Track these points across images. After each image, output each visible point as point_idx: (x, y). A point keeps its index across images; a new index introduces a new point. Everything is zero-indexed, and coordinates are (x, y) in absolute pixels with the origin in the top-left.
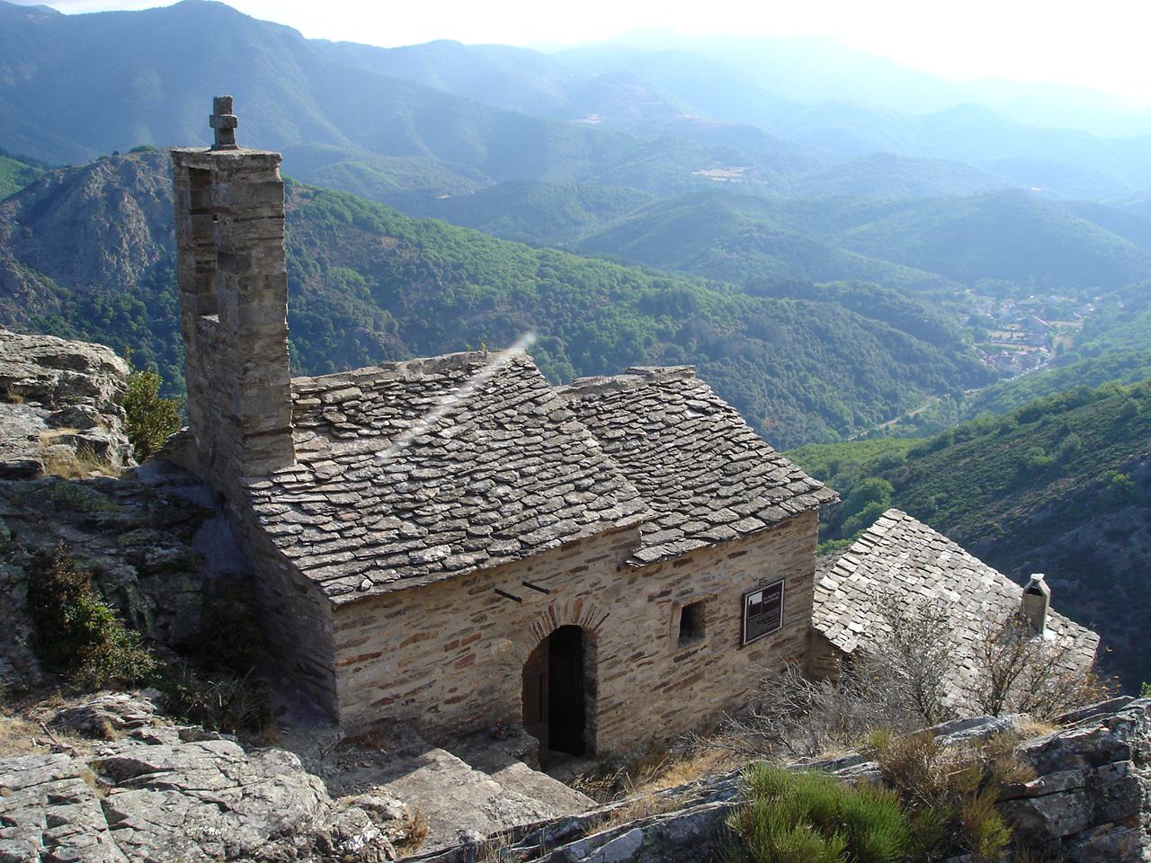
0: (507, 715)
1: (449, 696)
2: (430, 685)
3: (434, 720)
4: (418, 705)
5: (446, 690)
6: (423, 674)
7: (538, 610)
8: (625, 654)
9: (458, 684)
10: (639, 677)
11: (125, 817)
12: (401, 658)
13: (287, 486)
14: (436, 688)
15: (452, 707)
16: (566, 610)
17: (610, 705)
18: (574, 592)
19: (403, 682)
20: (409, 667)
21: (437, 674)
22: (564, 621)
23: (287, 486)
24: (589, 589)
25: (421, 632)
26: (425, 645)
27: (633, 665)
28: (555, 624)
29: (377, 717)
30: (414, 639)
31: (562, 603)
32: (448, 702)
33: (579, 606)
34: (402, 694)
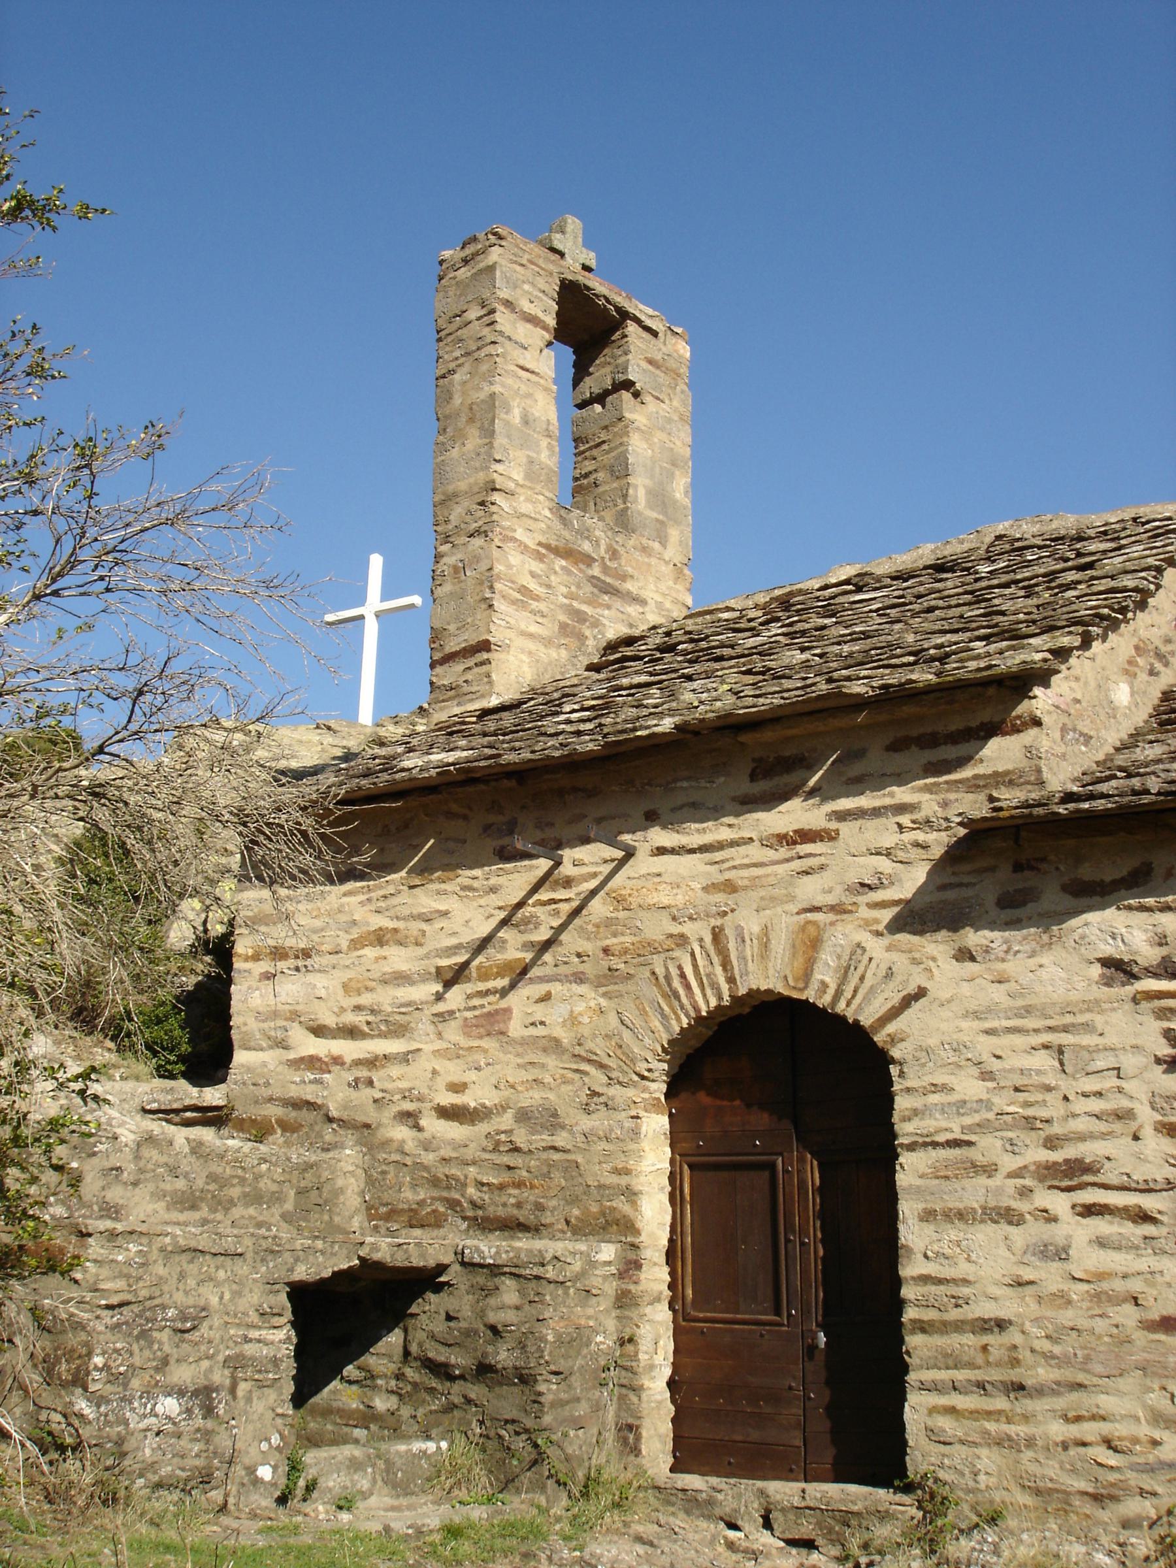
0: (594, 1208)
1: (448, 1099)
2: (405, 1058)
3: (410, 1146)
4: (378, 1095)
5: (441, 1083)
6: (398, 1030)
7: (675, 929)
8: (1012, 1147)
9: (472, 1076)
10: (1087, 1259)
11: (1165, 1072)
12: (350, 974)
13: (850, 587)
14: (423, 1065)
15: (453, 1131)
16: (765, 946)
17: (954, 1314)
18: (792, 898)
19: (351, 1032)
20: (366, 999)
21: (424, 1039)
22: (767, 976)
23: (850, 587)
24: (848, 899)
25: (391, 924)
26: (399, 959)
27: (1060, 1203)
28: (731, 980)
29: (294, 1092)
30: (380, 938)
31: (753, 926)
32: (447, 1113)
33: (810, 944)
34: (348, 1060)
